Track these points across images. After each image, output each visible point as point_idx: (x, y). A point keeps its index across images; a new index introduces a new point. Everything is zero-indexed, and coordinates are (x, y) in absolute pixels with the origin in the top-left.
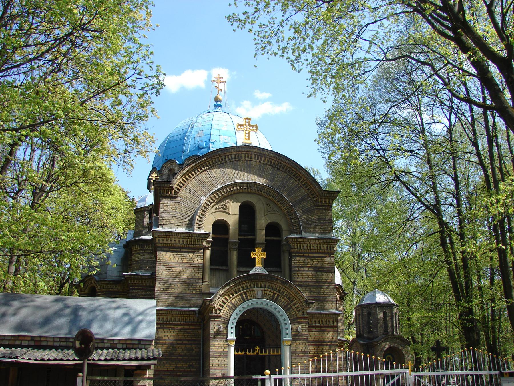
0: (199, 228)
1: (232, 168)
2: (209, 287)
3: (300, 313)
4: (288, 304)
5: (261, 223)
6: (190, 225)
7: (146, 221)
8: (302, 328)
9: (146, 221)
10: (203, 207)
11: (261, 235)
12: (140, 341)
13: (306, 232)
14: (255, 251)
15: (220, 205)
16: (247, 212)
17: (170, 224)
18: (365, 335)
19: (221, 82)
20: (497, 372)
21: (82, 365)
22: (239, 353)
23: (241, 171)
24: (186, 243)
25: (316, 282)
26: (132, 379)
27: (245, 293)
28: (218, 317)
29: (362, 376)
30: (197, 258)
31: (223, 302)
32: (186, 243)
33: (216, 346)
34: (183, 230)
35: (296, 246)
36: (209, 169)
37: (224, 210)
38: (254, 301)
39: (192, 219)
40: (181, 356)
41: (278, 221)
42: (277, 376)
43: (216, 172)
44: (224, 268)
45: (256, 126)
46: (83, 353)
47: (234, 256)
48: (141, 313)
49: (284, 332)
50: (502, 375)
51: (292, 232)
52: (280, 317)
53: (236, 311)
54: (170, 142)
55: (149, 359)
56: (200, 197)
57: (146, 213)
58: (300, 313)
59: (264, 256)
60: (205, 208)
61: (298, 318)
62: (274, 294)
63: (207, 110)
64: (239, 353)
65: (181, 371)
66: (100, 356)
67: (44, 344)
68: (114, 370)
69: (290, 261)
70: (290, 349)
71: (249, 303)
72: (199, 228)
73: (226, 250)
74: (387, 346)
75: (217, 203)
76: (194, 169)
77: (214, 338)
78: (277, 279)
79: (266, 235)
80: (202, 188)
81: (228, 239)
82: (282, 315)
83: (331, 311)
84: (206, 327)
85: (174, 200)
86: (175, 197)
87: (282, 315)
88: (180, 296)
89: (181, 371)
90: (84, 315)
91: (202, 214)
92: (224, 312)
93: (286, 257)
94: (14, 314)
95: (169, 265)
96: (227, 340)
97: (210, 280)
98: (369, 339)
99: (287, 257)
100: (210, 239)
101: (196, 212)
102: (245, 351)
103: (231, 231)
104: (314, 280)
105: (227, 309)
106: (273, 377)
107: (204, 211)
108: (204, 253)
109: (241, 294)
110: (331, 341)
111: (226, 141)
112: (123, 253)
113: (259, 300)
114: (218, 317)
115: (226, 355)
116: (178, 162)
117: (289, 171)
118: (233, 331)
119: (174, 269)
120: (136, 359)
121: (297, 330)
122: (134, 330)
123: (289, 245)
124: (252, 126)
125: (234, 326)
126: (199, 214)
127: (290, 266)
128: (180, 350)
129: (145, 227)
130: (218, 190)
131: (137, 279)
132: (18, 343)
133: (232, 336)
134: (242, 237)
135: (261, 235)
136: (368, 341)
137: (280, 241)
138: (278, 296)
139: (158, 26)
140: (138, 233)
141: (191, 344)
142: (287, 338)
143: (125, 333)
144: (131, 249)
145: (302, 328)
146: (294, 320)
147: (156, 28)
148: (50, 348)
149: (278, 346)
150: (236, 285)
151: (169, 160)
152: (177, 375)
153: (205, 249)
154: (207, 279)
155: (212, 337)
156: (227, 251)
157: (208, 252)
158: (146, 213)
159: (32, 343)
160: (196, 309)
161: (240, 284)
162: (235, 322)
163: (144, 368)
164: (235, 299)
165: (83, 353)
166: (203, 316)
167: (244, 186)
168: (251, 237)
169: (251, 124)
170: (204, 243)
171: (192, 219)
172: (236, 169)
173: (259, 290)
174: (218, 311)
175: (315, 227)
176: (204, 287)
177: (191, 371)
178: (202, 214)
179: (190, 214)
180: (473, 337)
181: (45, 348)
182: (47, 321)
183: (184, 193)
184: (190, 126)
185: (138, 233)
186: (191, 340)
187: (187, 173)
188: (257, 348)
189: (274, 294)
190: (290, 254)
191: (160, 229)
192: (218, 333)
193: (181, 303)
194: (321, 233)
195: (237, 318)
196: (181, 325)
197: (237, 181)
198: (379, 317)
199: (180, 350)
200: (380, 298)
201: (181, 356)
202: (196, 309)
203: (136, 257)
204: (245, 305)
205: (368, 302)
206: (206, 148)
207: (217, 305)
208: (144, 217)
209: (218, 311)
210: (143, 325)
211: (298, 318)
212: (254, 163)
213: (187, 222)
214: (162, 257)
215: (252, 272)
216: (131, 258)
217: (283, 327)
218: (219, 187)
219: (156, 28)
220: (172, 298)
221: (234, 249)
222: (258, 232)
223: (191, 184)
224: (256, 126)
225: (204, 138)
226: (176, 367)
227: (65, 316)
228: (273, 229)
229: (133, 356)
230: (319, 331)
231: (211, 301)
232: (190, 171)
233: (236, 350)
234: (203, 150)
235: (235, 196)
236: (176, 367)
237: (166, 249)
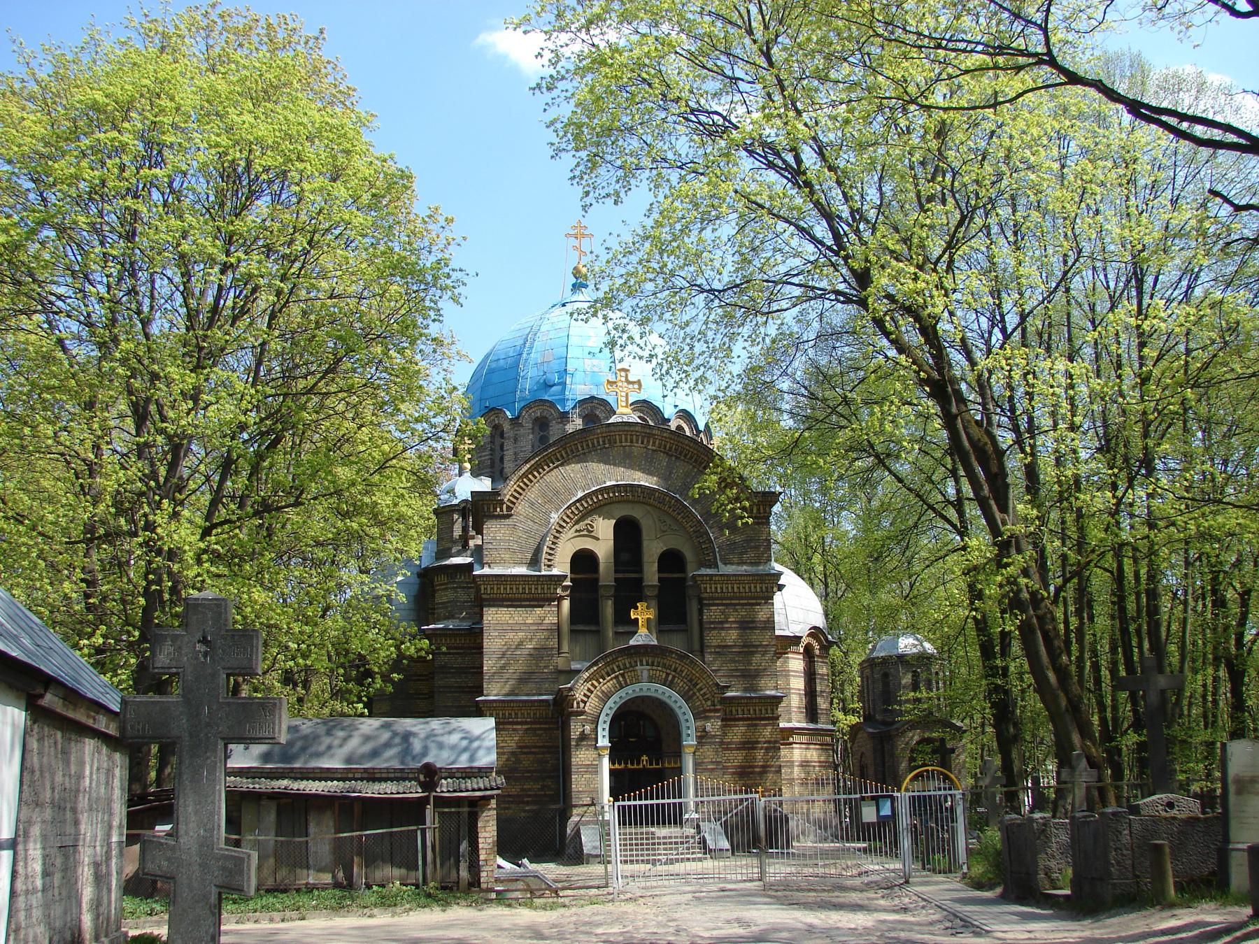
0: (549, 566)
1: (599, 462)
2: (569, 661)
3: (709, 703)
4: (690, 690)
5: (653, 549)
6: (534, 562)
7: (457, 531)
8: (713, 726)
9: (457, 531)
10: (551, 525)
11: (651, 574)
12: (480, 769)
13: (726, 564)
14: (636, 608)
15: (582, 525)
16: (627, 534)
17: (502, 562)
18: (878, 717)
19: (584, 236)
20: (858, 796)
21: (428, 797)
22: (617, 766)
23: (615, 465)
24: (528, 592)
25: (744, 646)
26: (906, 843)
27: (623, 675)
28: (583, 713)
29: (641, 806)
30: (547, 616)
31: (589, 690)
32: (528, 592)
33: (581, 757)
34: (522, 570)
35: (709, 588)
36: (562, 465)
37: (590, 533)
38: (637, 687)
39: (538, 551)
40: (528, 771)
41: (679, 548)
42: (621, 803)
43: (573, 471)
44: (593, 628)
45: (639, 382)
46: (429, 785)
47: (608, 609)
48: (478, 738)
49: (684, 732)
50: (863, 799)
51: (703, 564)
52: (677, 710)
53: (610, 703)
54: (491, 371)
55: (492, 789)
56: (547, 514)
57: (456, 516)
58: (709, 703)
59: (651, 614)
60: (558, 532)
61: (705, 711)
62: (668, 675)
63: (558, 300)
64: (617, 766)
65: (529, 796)
66: (445, 787)
67: (378, 776)
68: (458, 802)
69: (701, 612)
70: (694, 759)
71: (629, 689)
72: (549, 566)
73: (593, 597)
74: (916, 738)
75: (577, 522)
76: (537, 467)
77: (577, 745)
78: (672, 652)
79: (660, 570)
80: (552, 498)
81: (597, 580)
82: (680, 707)
83: (768, 692)
84: (565, 728)
85: (507, 522)
86: (508, 516)
87: (680, 707)
88: (524, 679)
89: (529, 796)
90: (417, 746)
91: (554, 543)
92: (591, 705)
93: (694, 606)
94: (341, 746)
95: (504, 629)
96: (596, 748)
97: (571, 651)
98: (884, 723)
99: (694, 606)
100: (568, 583)
101: (543, 539)
102: (626, 763)
103: (602, 567)
104: (740, 643)
105: (595, 700)
106: (617, 804)
107: (556, 537)
108: (558, 606)
109: (616, 677)
110: (769, 742)
111: (596, 369)
112: (417, 587)
113: (645, 685)
114: (583, 713)
115: (595, 769)
116: (508, 413)
117: (696, 461)
118: (606, 733)
119: (511, 635)
120: (480, 790)
121: (704, 730)
122: (472, 759)
123: (698, 587)
124: (633, 383)
125: (607, 726)
126: (548, 543)
127: (701, 622)
128: (526, 763)
129: (454, 542)
130: (578, 501)
131: (445, 635)
132: (350, 775)
133: (604, 741)
134: (620, 576)
135: (651, 574)
136: (884, 728)
137: (684, 580)
138: (674, 677)
139: (464, 238)
140: (443, 553)
141: (544, 753)
142: (690, 741)
143: (463, 762)
144: (432, 582)
145: (713, 726)
146: (699, 715)
147: (463, 243)
148: (386, 780)
149: (678, 754)
150: (607, 664)
151: (492, 409)
152: (523, 802)
153: (561, 599)
154: (565, 648)
155: (573, 743)
156: (597, 600)
157: (566, 604)
158: (456, 516)
159: (365, 775)
160: (550, 697)
161: (613, 661)
162: (609, 719)
163: (487, 799)
164: (607, 685)
165: (429, 785)
166: (560, 711)
167: (620, 492)
168: (633, 575)
169: (631, 378)
170: (559, 591)
171: (538, 551)
172: (605, 463)
173: (643, 670)
174: (582, 705)
175: (742, 553)
176: (560, 662)
177: (545, 795)
178: (554, 543)
179: (533, 544)
180: (1008, 730)
181: (380, 780)
182: (375, 753)
183: (521, 508)
184: (527, 341)
185: (443, 553)
186: (544, 747)
187: (525, 475)
188: (645, 758)
189: (668, 675)
190: (700, 601)
191: (487, 571)
192: (583, 736)
193: (526, 688)
194: (752, 564)
195: (611, 713)
196: (526, 723)
197: (608, 484)
198: (904, 682)
199: (527, 762)
200: (906, 644)
201: (528, 771)
202: (550, 697)
203: (443, 597)
204: (622, 693)
205: (882, 654)
206: (558, 384)
207: (579, 696)
208: (453, 523)
209: (582, 705)
210: (481, 753)
211: (705, 711)
212: (637, 449)
213: (529, 556)
214: (491, 616)
215: (632, 642)
216: (434, 597)
217: (684, 725)
218: (580, 494)
219: (463, 243)
220: (512, 682)
221: (608, 598)
222: (646, 568)
223: (533, 493)
224: (639, 382)
225: (556, 366)
226: (522, 790)
227: (396, 745)
228: (671, 560)
229: (475, 786)
230: (748, 726)
231: (570, 689)
232: (530, 471)
233: (612, 761)
234: (554, 388)
235: (606, 509)
236: (522, 790)
237: (498, 602)
